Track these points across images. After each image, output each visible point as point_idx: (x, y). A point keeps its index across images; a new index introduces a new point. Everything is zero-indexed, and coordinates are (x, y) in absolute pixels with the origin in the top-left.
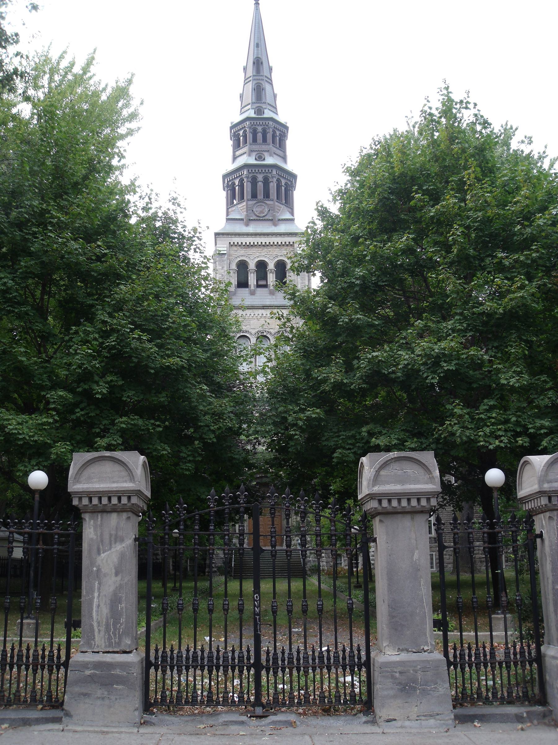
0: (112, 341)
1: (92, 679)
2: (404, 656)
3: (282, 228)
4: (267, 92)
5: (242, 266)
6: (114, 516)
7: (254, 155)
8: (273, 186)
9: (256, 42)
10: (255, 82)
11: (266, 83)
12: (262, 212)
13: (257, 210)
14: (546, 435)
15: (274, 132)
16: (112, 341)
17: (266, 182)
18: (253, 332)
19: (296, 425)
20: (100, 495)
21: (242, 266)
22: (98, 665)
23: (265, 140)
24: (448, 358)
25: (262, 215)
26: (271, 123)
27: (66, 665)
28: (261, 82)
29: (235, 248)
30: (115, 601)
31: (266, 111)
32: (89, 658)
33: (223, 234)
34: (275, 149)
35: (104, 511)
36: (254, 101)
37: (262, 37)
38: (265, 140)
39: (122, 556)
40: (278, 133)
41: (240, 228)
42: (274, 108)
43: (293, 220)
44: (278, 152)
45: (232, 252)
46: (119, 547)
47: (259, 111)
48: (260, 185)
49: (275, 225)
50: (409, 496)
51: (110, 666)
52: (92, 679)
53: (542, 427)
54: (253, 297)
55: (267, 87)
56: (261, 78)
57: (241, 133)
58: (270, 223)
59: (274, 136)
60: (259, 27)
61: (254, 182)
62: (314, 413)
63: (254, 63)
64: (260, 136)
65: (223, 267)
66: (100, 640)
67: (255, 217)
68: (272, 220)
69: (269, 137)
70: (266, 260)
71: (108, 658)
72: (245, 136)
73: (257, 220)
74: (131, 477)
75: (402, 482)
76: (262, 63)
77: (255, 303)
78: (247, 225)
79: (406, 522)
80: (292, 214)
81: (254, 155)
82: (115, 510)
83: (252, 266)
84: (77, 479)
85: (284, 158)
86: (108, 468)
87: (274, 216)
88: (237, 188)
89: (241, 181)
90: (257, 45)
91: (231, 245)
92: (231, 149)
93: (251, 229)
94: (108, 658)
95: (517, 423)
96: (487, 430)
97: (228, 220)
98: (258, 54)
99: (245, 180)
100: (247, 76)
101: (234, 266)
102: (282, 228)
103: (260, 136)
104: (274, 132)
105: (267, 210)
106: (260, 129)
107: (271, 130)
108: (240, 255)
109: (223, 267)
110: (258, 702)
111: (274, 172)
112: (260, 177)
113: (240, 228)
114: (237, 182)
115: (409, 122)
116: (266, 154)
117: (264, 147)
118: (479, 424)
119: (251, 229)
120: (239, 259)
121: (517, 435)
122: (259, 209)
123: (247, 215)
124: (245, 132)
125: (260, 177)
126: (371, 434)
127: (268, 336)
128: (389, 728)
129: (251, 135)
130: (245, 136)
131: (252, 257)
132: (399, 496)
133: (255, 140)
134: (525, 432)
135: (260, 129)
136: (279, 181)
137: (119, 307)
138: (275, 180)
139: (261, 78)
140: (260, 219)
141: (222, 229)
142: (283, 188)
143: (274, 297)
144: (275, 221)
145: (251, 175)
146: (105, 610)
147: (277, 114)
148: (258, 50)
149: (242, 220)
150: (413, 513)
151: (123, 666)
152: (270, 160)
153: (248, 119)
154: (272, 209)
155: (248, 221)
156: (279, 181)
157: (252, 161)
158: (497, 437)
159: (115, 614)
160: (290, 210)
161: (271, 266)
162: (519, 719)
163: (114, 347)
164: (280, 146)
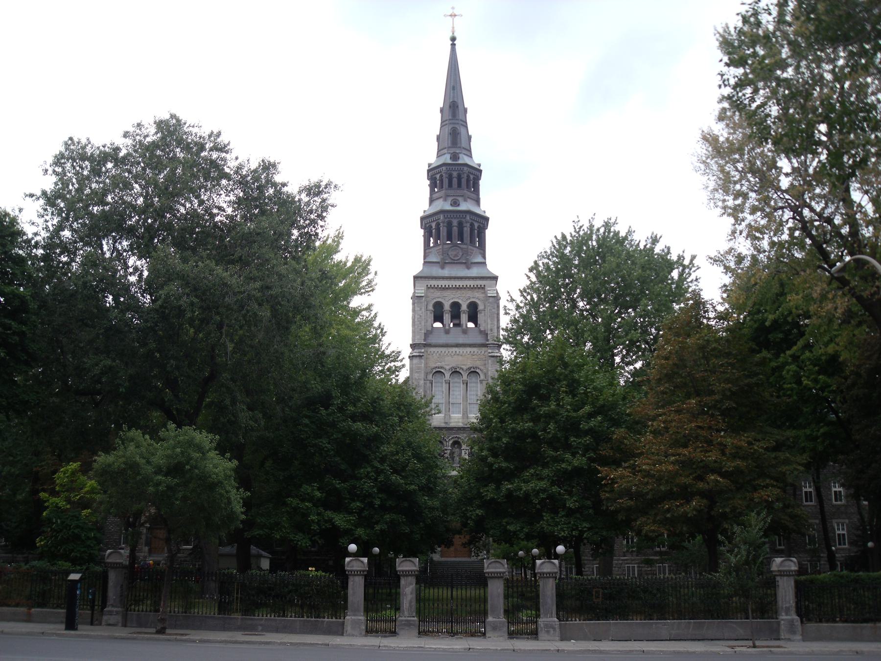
0: (381, 478)
1: (404, 624)
2: (494, 619)
3: (475, 272)
4: (462, 136)
5: (438, 306)
6: (410, 577)
7: (450, 200)
8: (467, 230)
9: (452, 84)
10: (451, 126)
11: (461, 127)
12: (456, 256)
13: (452, 253)
14: (586, 531)
15: (468, 176)
16: (381, 478)
17: (461, 225)
18: (448, 368)
19: (471, 518)
20: (406, 571)
21: (438, 306)
22: (406, 621)
23: (459, 185)
24: (544, 490)
25: (456, 258)
26: (465, 168)
27: (395, 621)
28: (458, 198)
29: (432, 291)
30: (411, 602)
31: (461, 155)
32: (403, 618)
33: (421, 277)
34: (469, 193)
35: (407, 576)
36: (450, 145)
37: (458, 79)
38: (459, 185)
39: (412, 590)
40: (472, 177)
41: (437, 271)
42: (469, 152)
43: (485, 263)
44: (473, 195)
45: (429, 294)
46: (411, 587)
47: (455, 157)
48: (455, 230)
49: (468, 268)
50: (497, 573)
51: (410, 621)
52: (405, 625)
53: (585, 527)
54: (448, 336)
55: (463, 130)
56: (457, 122)
57: (438, 176)
58: (464, 266)
59: (468, 181)
60: (455, 69)
61: (449, 225)
62: (479, 512)
63: (450, 107)
64: (455, 181)
65: (421, 309)
66: (406, 613)
67: (450, 261)
68: (465, 263)
69: (464, 181)
70: (460, 301)
71: (409, 618)
72: (441, 181)
73: (451, 263)
74: (415, 566)
75: (495, 568)
76: (457, 107)
77: (450, 342)
78: (443, 268)
79: (496, 580)
80: (484, 257)
81: (450, 200)
82: (410, 575)
83: (447, 306)
84: (399, 566)
85: (477, 201)
86: (408, 563)
87: (467, 259)
88: (434, 231)
89: (438, 225)
90: (454, 88)
91: (428, 288)
92: (428, 189)
93: (446, 272)
94: (409, 618)
95: (574, 525)
96: (559, 527)
97: (425, 263)
98: (454, 97)
99: (441, 224)
100: (445, 119)
101: (431, 307)
102: (475, 272)
103: (455, 181)
104: (468, 176)
105: (461, 254)
106: (455, 174)
107: (466, 175)
108: (437, 296)
109: (421, 309)
110: (452, 632)
111: (468, 218)
112: (455, 223)
113: (437, 271)
114: (434, 225)
115: (576, 225)
116: (460, 199)
117: (459, 192)
118: (557, 524)
119: (446, 272)
120: (435, 301)
121: (574, 530)
122: (454, 253)
123: (443, 259)
124: (441, 176)
125: (455, 223)
126: (508, 523)
127: (461, 371)
128: (489, 639)
129: (447, 180)
130: (441, 181)
131: (447, 299)
132: (494, 573)
133: (450, 185)
134: (577, 529)
135: (455, 174)
136: (472, 225)
137: (382, 460)
138: (468, 225)
139: (457, 122)
140: (454, 262)
141: (421, 272)
142: (476, 231)
143: (466, 336)
144: (468, 265)
145: (446, 220)
146: (408, 605)
147: (471, 157)
148: (454, 93)
149: (438, 263)
150: (499, 578)
151: (413, 621)
152: (464, 206)
153: (444, 165)
154: (466, 253)
155: (443, 265)
156: (472, 225)
157: (448, 207)
158: (564, 531)
159: (410, 606)
160: (482, 251)
161: (464, 307)
162: (528, 638)
163: (383, 481)
164: (471, 242)
